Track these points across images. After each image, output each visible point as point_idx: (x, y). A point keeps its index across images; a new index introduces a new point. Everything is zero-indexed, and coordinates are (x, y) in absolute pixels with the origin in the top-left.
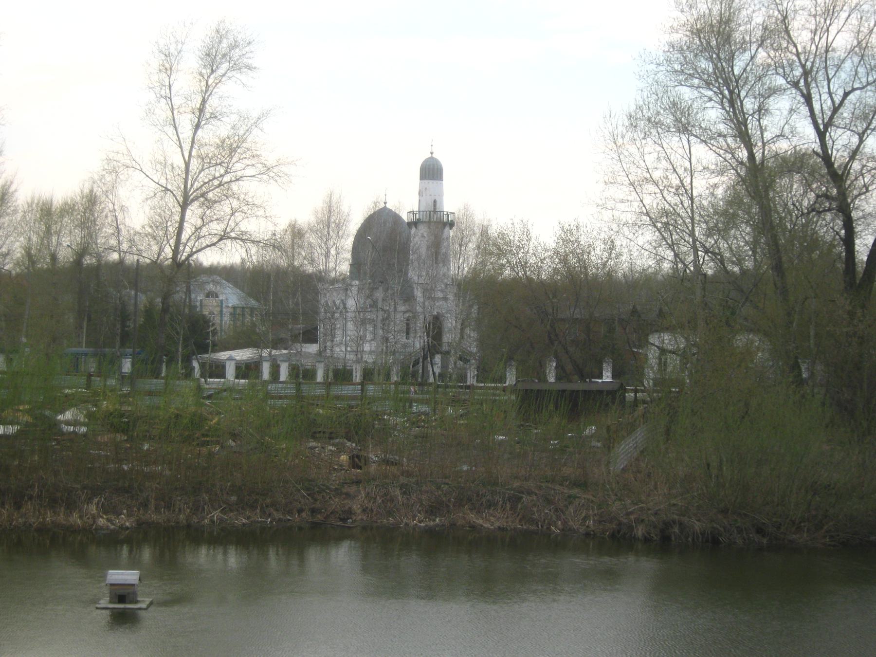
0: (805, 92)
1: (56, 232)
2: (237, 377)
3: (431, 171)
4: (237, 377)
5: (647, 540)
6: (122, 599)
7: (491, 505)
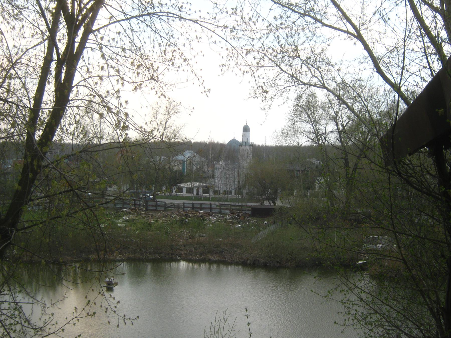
0: (356, 34)
1: (313, 106)
2: (186, 193)
3: (246, 129)
4: (186, 193)
5: (250, 264)
6: (109, 284)
7: (216, 253)
